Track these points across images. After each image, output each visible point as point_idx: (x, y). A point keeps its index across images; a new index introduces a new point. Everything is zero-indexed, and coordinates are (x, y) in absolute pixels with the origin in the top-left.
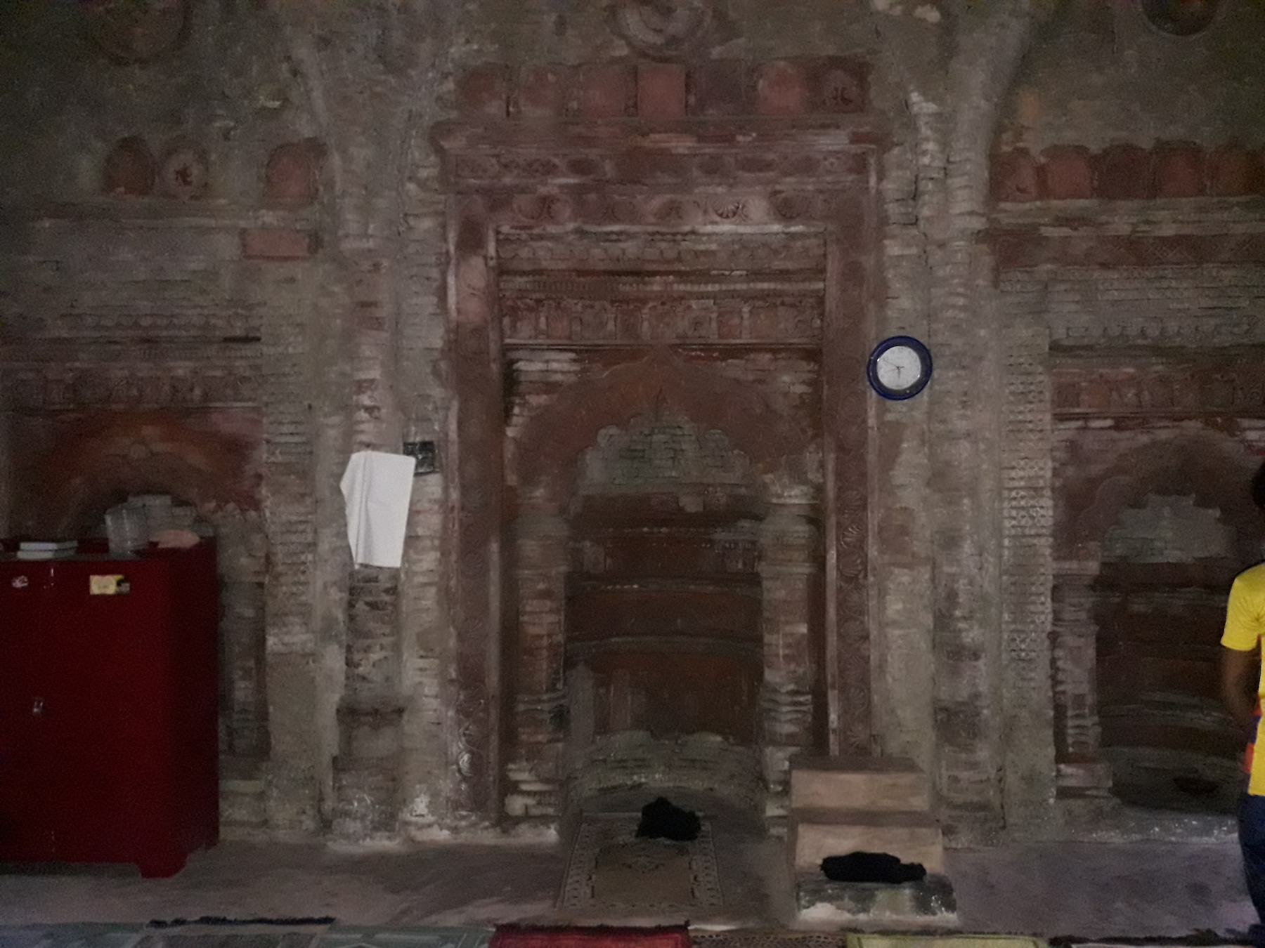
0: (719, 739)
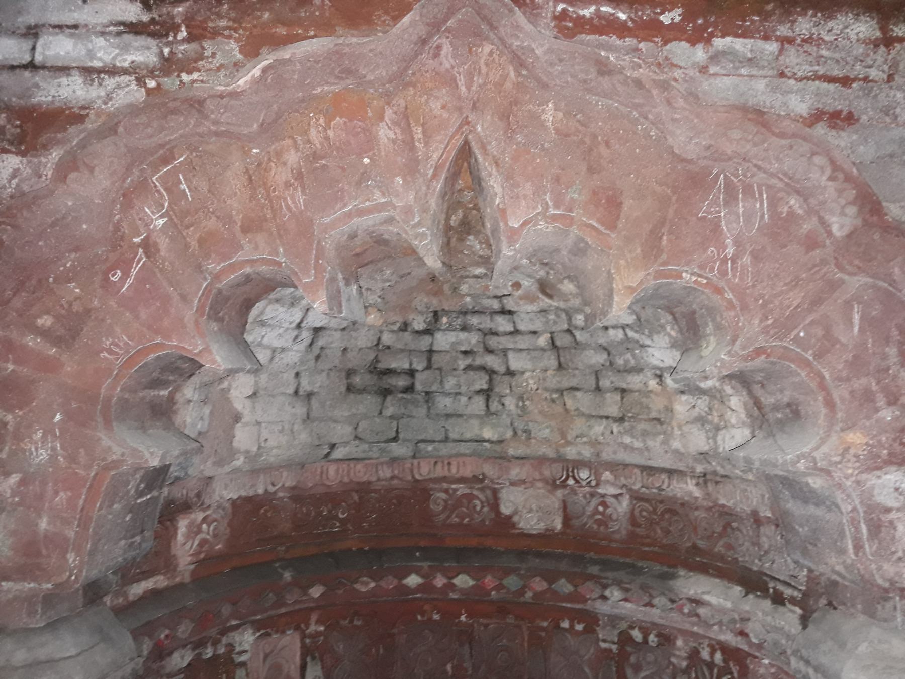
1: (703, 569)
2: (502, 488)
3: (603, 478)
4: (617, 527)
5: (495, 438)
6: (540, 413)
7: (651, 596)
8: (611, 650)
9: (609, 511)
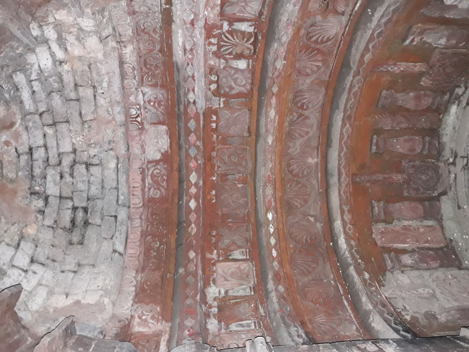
0: (454, 109)
1: (170, 47)
2: (146, 158)
3: (135, 101)
4: (160, 95)
5: (115, 161)
6: (98, 134)
7: (189, 77)
8: (224, 101)
9: (152, 99)
